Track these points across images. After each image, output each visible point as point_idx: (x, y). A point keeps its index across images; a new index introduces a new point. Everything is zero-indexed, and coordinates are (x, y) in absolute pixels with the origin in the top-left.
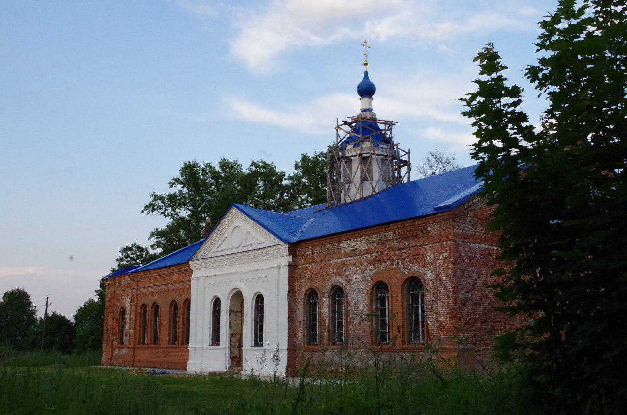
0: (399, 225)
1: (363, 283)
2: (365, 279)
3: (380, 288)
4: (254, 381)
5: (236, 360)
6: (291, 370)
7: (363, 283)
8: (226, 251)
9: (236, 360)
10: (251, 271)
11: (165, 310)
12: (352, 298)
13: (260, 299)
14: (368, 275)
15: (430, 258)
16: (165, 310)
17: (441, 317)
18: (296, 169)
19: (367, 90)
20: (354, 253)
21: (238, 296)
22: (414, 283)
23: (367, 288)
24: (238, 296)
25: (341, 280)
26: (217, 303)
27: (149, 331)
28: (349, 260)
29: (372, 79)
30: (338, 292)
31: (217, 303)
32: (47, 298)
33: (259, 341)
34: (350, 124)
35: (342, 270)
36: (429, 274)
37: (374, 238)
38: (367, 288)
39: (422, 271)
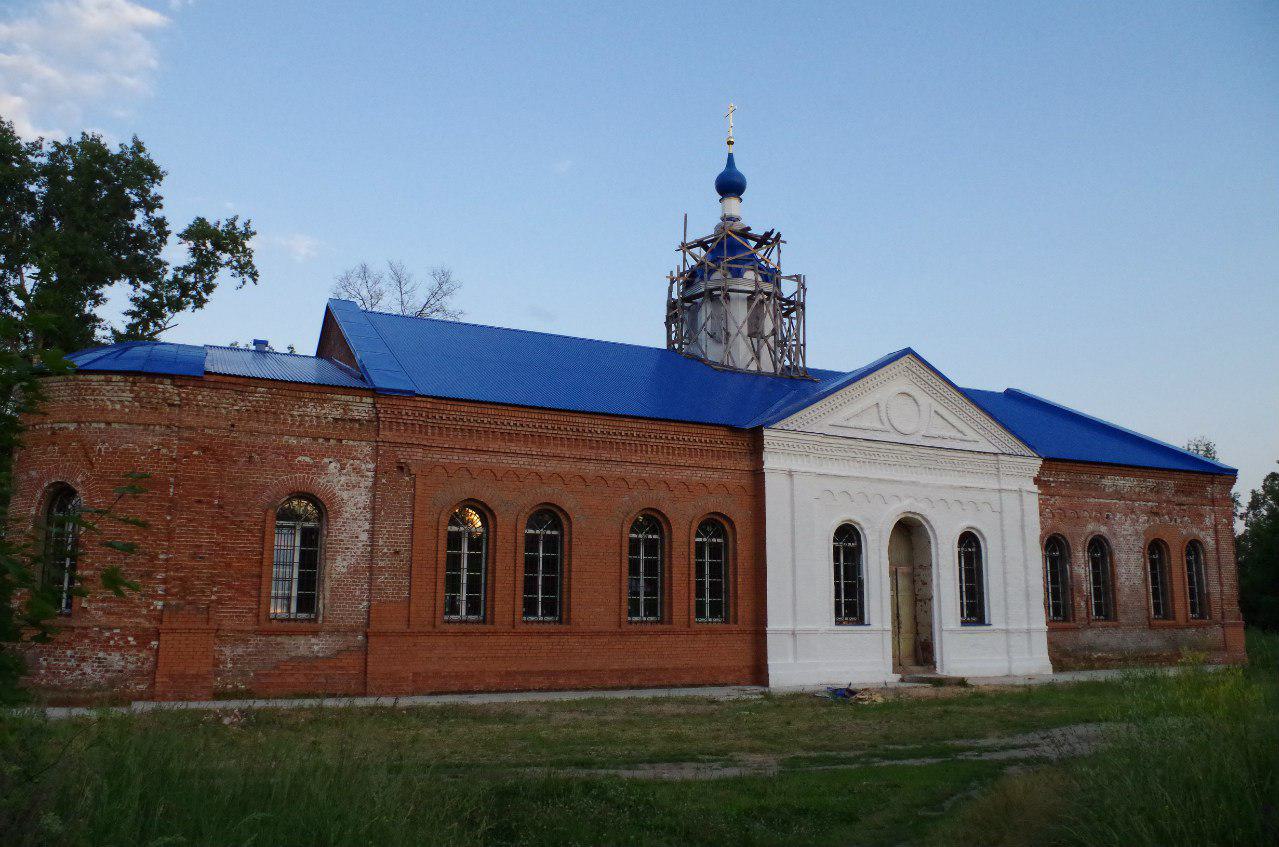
0: (1183, 475)
1: (1134, 537)
2: (1137, 533)
3: (1156, 549)
4: (967, 695)
5: (918, 649)
6: (1060, 659)
7: (1134, 537)
8: (939, 440)
9: (918, 649)
10: (952, 487)
11: (683, 538)
12: (1120, 556)
13: (970, 542)
14: (1141, 528)
15: (1208, 521)
16: (683, 538)
17: (1226, 589)
18: (199, 232)
19: (730, 185)
20: (1118, 495)
21: (909, 532)
22: (1194, 547)
23: (1140, 545)
24: (909, 532)
25: (1103, 529)
26: (848, 538)
27: (676, 576)
28: (1116, 503)
29: (740, 166)
30: (1099, 548)
31: (848, 538)
32: (936, 412)
33: (974, 611)
34: (705, 246)
35: (1104, 514)
36: (1209, 539)
37: (1151, 482)
38: (1140, 545)
39: (1202, 535)
